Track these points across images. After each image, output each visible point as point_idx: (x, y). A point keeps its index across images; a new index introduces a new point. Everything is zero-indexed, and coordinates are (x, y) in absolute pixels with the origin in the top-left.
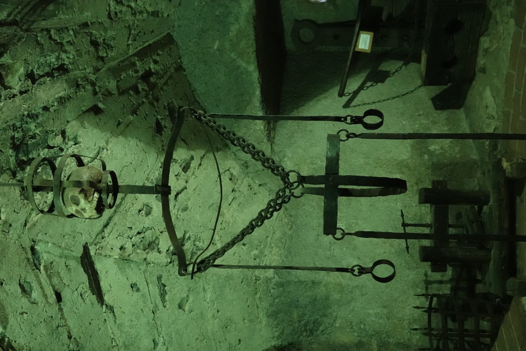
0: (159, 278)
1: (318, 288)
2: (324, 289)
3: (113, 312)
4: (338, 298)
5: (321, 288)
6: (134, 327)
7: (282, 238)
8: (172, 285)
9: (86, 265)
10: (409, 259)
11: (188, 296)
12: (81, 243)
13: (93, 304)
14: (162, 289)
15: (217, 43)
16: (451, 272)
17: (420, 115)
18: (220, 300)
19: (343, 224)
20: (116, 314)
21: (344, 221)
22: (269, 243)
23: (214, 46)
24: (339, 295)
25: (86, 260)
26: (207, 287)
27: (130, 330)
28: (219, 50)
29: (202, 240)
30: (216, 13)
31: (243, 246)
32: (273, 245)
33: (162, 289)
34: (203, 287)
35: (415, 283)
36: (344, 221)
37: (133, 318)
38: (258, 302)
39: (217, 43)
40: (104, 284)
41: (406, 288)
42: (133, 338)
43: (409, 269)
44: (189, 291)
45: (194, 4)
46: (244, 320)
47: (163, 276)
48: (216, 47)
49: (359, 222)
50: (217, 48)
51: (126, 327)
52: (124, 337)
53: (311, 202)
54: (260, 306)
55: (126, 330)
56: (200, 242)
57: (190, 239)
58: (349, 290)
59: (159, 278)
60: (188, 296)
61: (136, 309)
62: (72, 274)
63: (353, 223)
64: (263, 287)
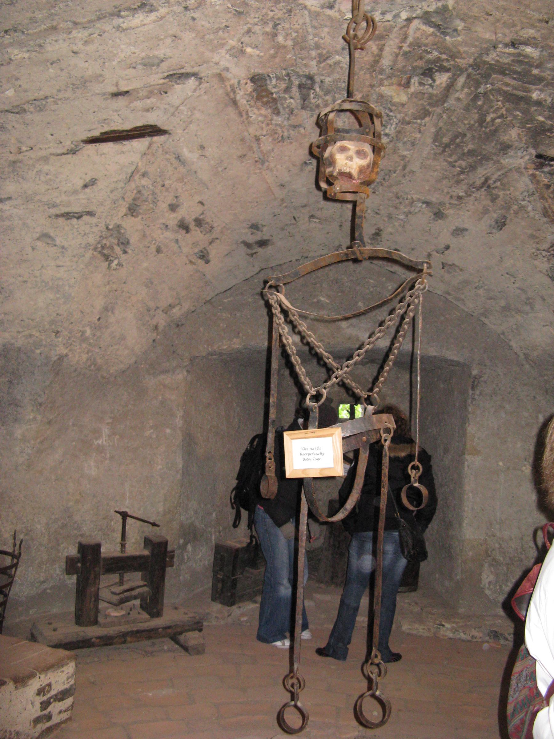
0: (90, 214)
1: (32, 410)
2: (31, 417)
3: (67, 154)
4: (16, 435)
5: (32, 414)
6: (38, 177)
7: (95, 365)
8: (77, 228)
9: (143, 130)
10: (60, 524)
11: (55, 245)
12: (174, 129)
13: (90, 131)
14: (75, 215)
15: (327, 301)
16: (381, 506)
17: (219, 532)
18: (39, 285)
19: (104, 442)
20: (63, 156)
21: (109, 443)
22: (93, 349)
23: (324, 297)
24: (19, 437)
25: (150, 130)
26: (62, 269)
27: (35, 171)
28: (318, 302)
29: (118, 267)
30: (360, 303)
31: (98, 317)
32: (90, 354)
33: (75, 215)
34: (63, 266)
35: (30, 531)
36: (109, 443)
37: (50, 177)
38: (27, 333)
39: (327, 301)
40: (108, 147)
41: (25, 521)
42: (23, 173)
43: (47, 524)
44: (63, 248)
45: (371, 279)
46: (5, 314)
47: (93, 218)
48: (322, 299)
49: (107, 461)
50: (321, 301)
51: (41, 167)
52: (29, 163)
53: (132, 402)
54: (20, 335)
55: (37, 166)
56: (116, 265)
57: (124, 253)
58: (26, 449)
59: (90, 214)
60: (55, 245)
61: (60, 182)
62: (140, 112)
63: (106, 454)
64: (46, 341)
